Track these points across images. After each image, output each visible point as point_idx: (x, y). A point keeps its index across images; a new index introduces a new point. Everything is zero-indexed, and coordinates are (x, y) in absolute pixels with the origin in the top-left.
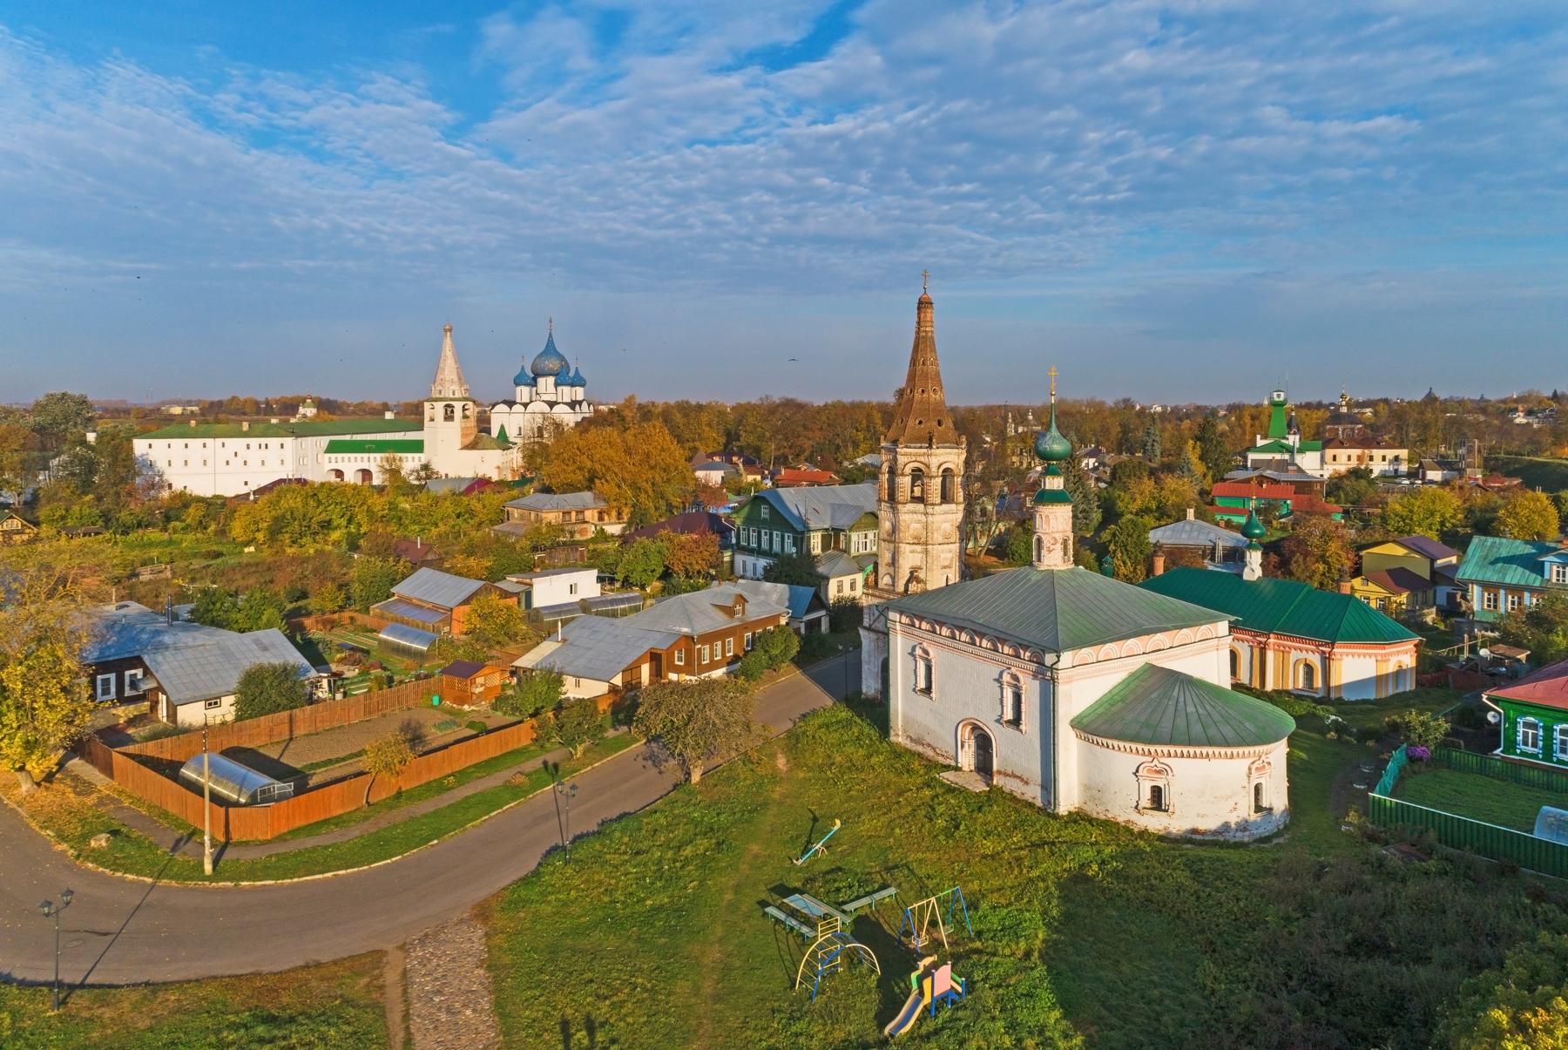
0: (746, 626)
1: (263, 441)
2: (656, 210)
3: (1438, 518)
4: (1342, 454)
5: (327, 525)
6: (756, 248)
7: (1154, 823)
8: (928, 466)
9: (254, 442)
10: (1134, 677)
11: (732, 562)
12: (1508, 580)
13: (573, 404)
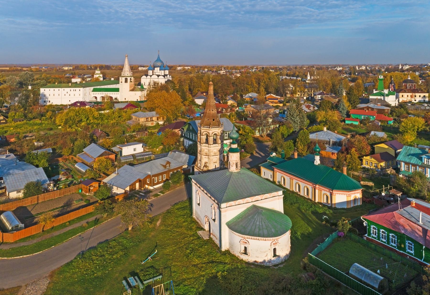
0: (170, 171)
1: (75, 89)
2: (209, 4)
3: (416, 127)
4: (405, 95)
5: (81, 121)
6: (240, 15)
7: (244, 258)
8: (209, 133)
9: (72, 89)
10: (248, 209)
11: (183, 141)
12: (412, 162)
13: (164, 76)
